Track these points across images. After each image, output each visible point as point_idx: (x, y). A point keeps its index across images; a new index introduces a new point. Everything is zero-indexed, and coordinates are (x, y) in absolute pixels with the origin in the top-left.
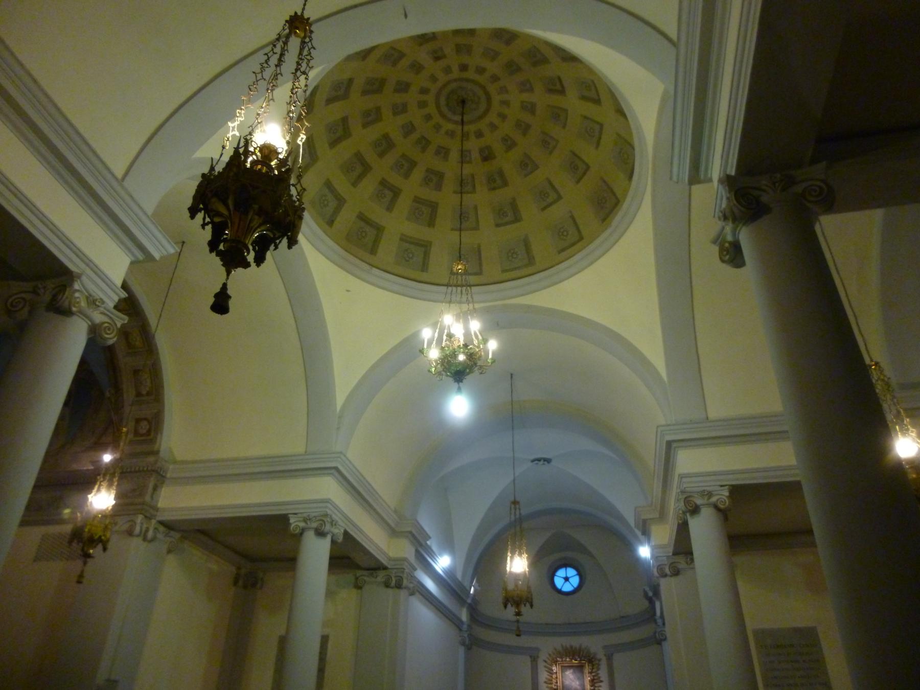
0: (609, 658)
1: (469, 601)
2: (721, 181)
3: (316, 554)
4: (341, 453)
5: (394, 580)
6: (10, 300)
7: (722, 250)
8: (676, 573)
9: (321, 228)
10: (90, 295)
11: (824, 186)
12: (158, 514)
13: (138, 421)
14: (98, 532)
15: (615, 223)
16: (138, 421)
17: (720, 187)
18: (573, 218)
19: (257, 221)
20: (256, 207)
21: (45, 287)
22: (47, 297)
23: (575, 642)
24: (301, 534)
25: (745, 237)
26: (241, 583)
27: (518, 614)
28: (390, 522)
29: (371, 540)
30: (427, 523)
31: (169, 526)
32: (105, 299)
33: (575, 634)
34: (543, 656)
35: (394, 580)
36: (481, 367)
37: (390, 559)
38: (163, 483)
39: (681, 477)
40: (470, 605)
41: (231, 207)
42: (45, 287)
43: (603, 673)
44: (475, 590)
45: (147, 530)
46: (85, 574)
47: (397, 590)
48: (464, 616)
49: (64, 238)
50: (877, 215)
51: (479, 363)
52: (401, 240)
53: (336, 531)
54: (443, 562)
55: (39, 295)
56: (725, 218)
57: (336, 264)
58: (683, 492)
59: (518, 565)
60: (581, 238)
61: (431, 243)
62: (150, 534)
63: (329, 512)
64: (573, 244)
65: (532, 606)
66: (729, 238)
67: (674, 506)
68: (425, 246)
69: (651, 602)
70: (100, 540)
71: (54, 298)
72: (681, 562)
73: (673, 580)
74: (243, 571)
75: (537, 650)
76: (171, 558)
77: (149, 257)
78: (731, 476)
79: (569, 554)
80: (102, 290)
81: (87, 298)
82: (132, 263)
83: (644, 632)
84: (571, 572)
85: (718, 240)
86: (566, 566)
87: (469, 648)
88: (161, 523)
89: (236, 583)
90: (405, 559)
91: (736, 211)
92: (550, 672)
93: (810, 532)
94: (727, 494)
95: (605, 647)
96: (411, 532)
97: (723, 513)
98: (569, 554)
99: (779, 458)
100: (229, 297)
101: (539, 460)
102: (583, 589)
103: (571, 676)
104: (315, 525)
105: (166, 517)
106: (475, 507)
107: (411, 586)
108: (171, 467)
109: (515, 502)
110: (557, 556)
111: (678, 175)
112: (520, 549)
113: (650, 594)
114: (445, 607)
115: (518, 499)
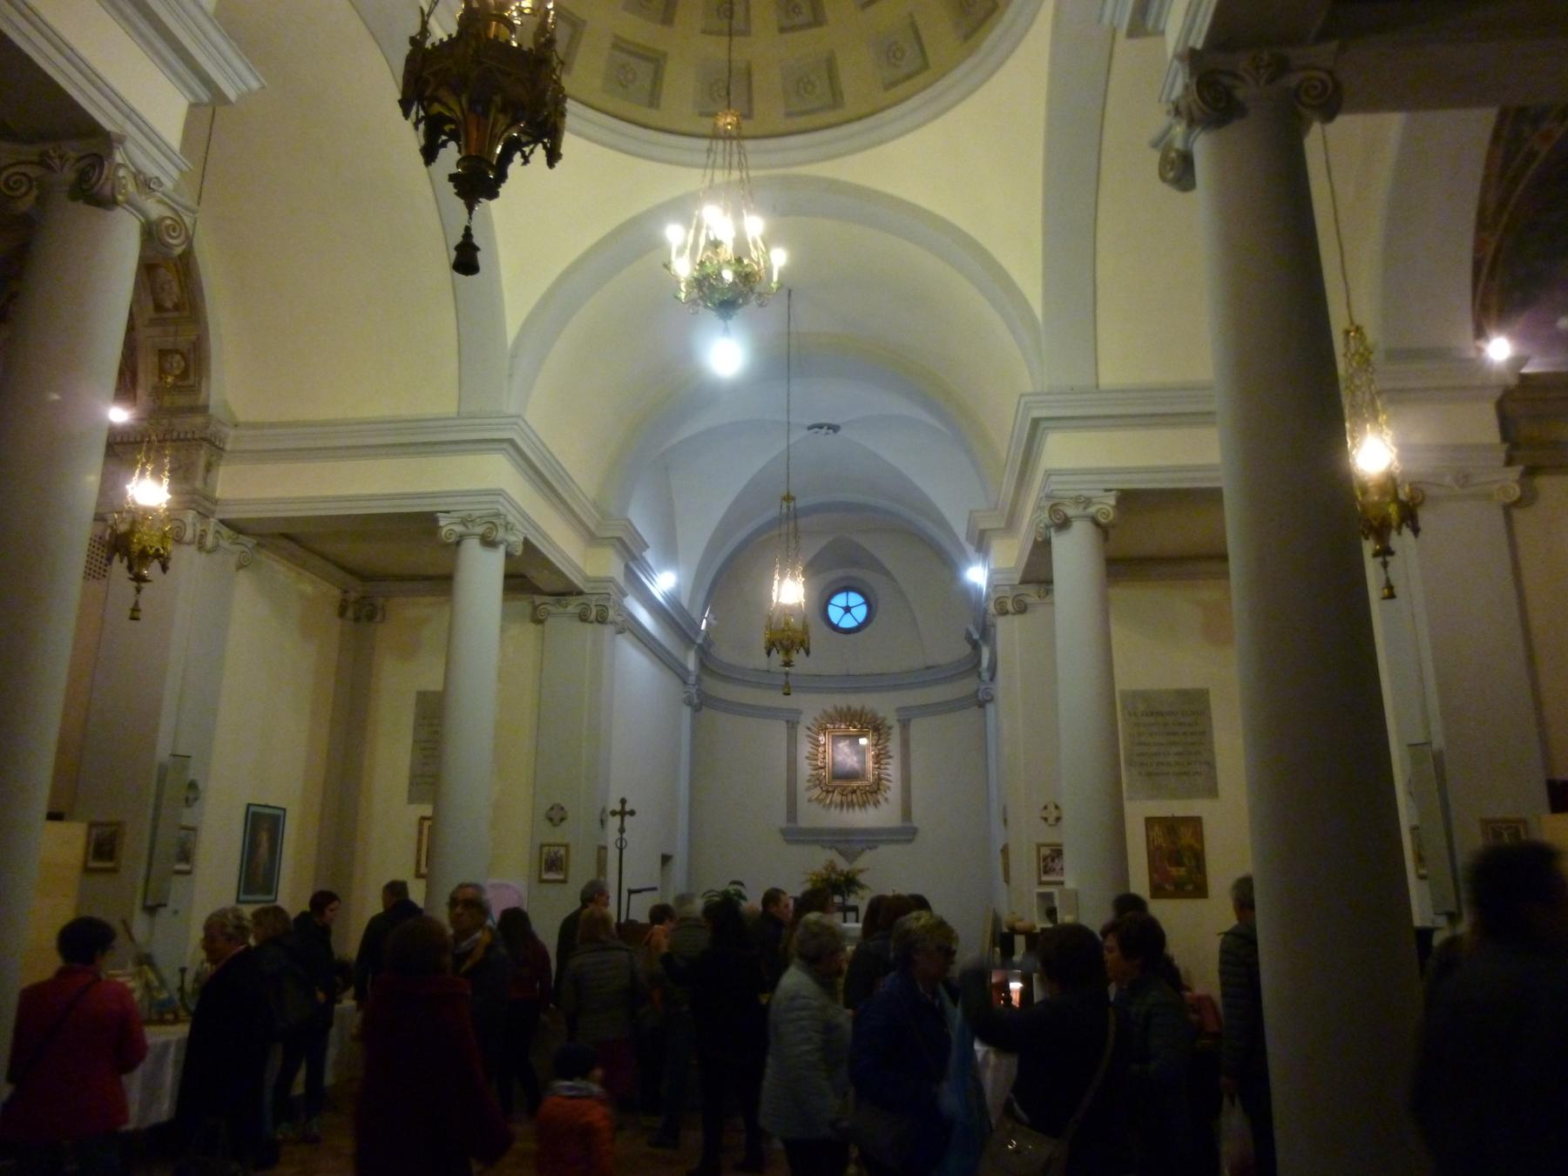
0: (905, 725)
2: (1178, 56)
3: (483, 574)
4: (519, 416)
6: (12, 170)
7: (1165, 163)
8: (1022, 609)
10: (140, 172)
11: (1330, 83)
13: (163, 354)
14: (153, 543)
15: (986, 46)
16: (163, 354)
17: (1176, 63)
18: (913, 25)
19: (503, 120)
20: (498, 99)
21: (61, 157)
22: (69, 175)
23: (855, 701)
24: (458, 543)
25: (1203, 147)
26: (350, 613)
27: (787, 664)
30: (641, 520)
31: (236, 527)
32: (163, 179)
34: (806, 720)
36: (760, 294)
37: (588, 579)
38: (221, 457)
39: (1049, 473)
40: (700, 646)
41: (465, 106)
43: (894, 746)
44: (708, 624)
45: (203, 536)
46: (141, 606)
47: (597, 625)
48: (691, 662)
50: (1393, 124)
51: (758, 288)
52: (615, 46)
53: (512, 539)
54: (664, 583)
55: (49, 168)
56: (1177, 112)
59: (789, 591)
60: (925, 66)
61: (665, 55)
62: (210, 541)
63: (503, 510)
64: (909, 77)
65: (808, 653)
66: (1178, 144)
67: (1030, 516)
68: (656, 61)
69: (976, 646)
70: (157, 555)
71: (83, 176)
72: (1031, 594)
74: (353, 595)
75: (799, 712)
77: (218, 96)
79: (854, 572)
80: (154, 161)
81: (135, 177)
82: (192, 106)
83: (965, 687)
84: (855, 599)
85: (1161, 142)
86: (847, 589)
87: (696, 709)
88: (222, 521)
89: (342, 613)
90: (611, 580)
91: (1194, 107)
92: (816, 744)
93: (1223, 558)
94: (1113, 502)
95: (899, 710)
96: (620, 540)
97: (1103, 530)
98: (854, 572)
99: (1199, 453)
100: (476, 249)
101: (821, 426)
103: (847, 750)
104: (480, 530)
105: (233, 514)
106: (712, 499)
107: (619, 619)
108: (232, 433)
109: (788, 498)
110: (841, 573)
111: (1113, 15)
112: (793, 568)
113: (976, 636)
114: (668, 653)
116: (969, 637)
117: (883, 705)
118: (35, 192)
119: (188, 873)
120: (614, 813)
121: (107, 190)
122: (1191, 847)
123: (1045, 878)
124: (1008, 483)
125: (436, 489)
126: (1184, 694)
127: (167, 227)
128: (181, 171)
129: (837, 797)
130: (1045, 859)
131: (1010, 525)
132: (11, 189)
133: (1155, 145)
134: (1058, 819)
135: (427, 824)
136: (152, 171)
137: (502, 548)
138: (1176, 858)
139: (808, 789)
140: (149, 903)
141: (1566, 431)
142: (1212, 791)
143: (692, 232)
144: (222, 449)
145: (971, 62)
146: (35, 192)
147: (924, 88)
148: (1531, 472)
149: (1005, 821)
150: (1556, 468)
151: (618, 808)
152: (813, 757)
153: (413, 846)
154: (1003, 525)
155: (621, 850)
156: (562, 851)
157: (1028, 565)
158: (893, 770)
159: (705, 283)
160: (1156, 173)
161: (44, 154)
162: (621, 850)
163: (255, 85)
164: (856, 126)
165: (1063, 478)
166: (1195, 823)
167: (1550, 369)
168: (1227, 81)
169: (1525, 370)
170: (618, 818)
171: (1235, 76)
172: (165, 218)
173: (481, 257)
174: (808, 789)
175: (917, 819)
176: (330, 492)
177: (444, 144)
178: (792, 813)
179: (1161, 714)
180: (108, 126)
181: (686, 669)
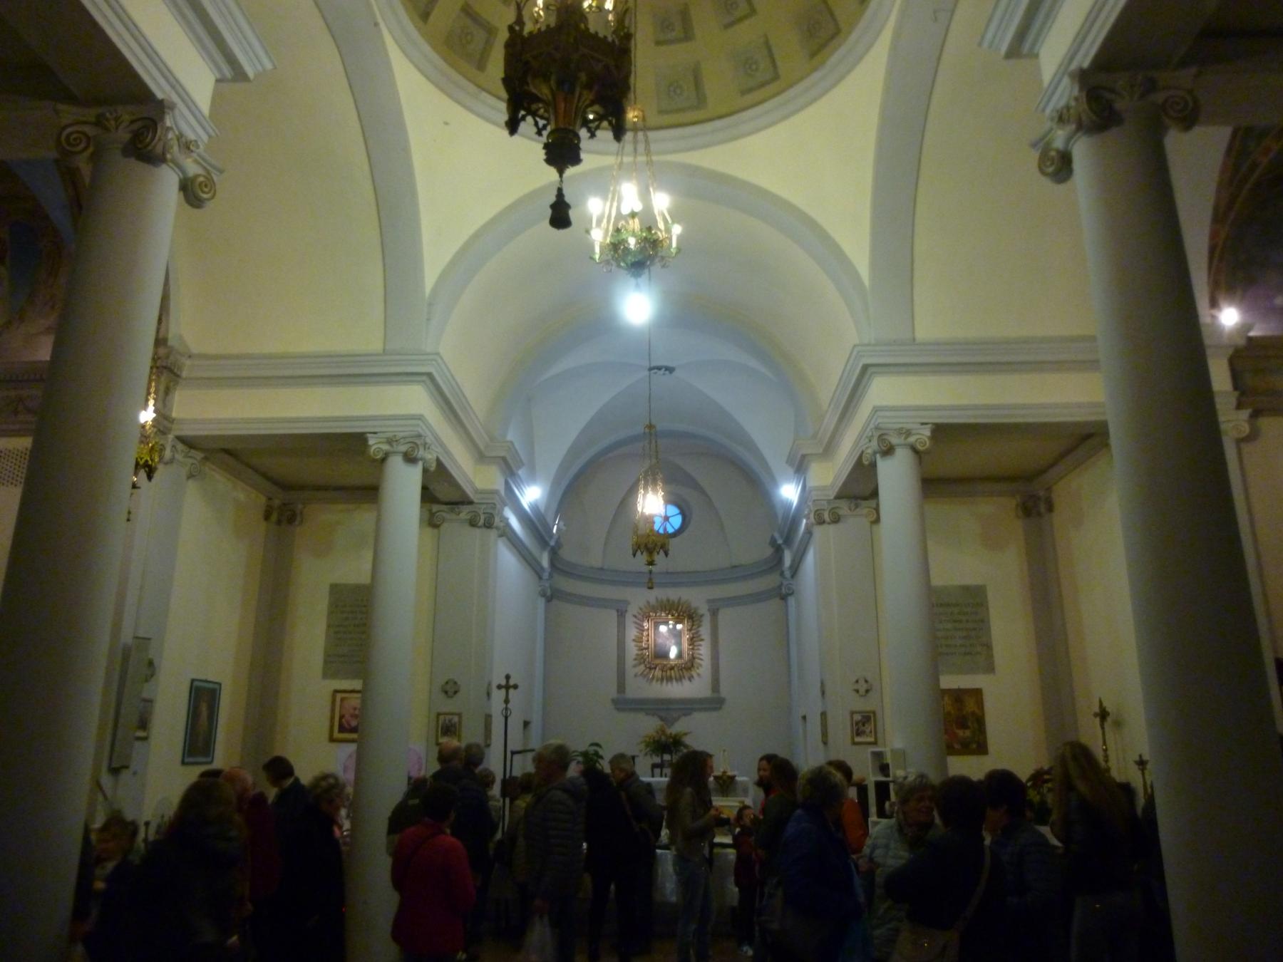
0: (714, 613)
1: (552, 543)
3: (404, 486)
5: (482, 517)
6: (69, 130)
8: (836, 520)
9: (412, 20)
11: (1191, 104)
12: (174, 426)
21: (116, 119)
22: (124, 135)
23: (673, 594)
24: (383, 460)
25: (1082, 151)
26: (274, 517)
28: (478, 441)
29: (459, 467)
33: (675, 585)
34: (633, 610)
35: (482, 517)
36: (663, 258)
37: (477, 491)
38: (177, 383)
42: (116, 119)
43: (705, 631)
47: (484, 530)
48: (545, 562)
49: (150, 51)
54: (532, 495)
55: (107, 129)
57: (432, 82)
58: (877, 428)
60: (776, 77)
64: (763, 85)
65: (666, 554)
66: (1059, 144)
69: (778, 551)
73: (831, 529)
74: (277, 502)
75: (627, 603)
76: (190, 482)
78: (956, 413)
82: (218, 81)
87: (549, 600)
88: (181, 439)
89: (267, 517)
92: (641, 629)
94: (928, 433)
95: (709, 601)
101: (659, 368)
102: (685, 534)
104: (403, 448)
105: (188, 431)
108: (188, 362)
109: (651, 426)
112: (654, 483)
113: (780, 541)
114: (527, 549)
115: (654, 422)
116: (773, 542)
117: (696, 597)
118: (91, 149)
119: (145, 739)
120: (499, 687)
121: (159, 149)
122: (973, 713)
123: (858, 739)
124: (830, 421)
125: (364, 413)
126: (966, 589)
127: (201, 184)
128: (210, 136)
129: (658, 673)
130: (857, 723)
131: (828, 450)
132: (69, 144)
133: (1034, 145)
134: (867, 691)
135: (339, 696)
136: (191, 136)
137: (420, 465)
138: (962, 724)
139: (635, 666)
140: (114, 765)
141: (1282, 382)
142: (990, 668)
143: (608, 204)
144: (178, 376)
145: (816, 76)
146: (91, 149)
147: (778, 94)
148: (1256, 414)
149: (823, 693)
150: (1275, 412)
151: (503, 682)
152: (638, 640)
153: (327, 713)
154: (821, 451)
155: (506, 718)
156: (456, 719)
157: (845, 484)
158: (704, 650)
159: (616, 247)
160: (1035, 164)
161: (103, 115)
162: (506, 718)
163: (269, 66)
164: (718, 123)
165: (888, 414)
166: (977, 693)
167: (1269, 333)
168: (1108, 95)
169: (1252, 334)
170: (503, 691)
171: (1112, 91)
172: (198, 176)
173: (572, 214)
174: (635, 666)
175: (725, 691)
176: (292, 414)
177: (523, 118)
178: (621, 687)
179: (948, 605)
180: (160, 95)
181: (542, 568)
